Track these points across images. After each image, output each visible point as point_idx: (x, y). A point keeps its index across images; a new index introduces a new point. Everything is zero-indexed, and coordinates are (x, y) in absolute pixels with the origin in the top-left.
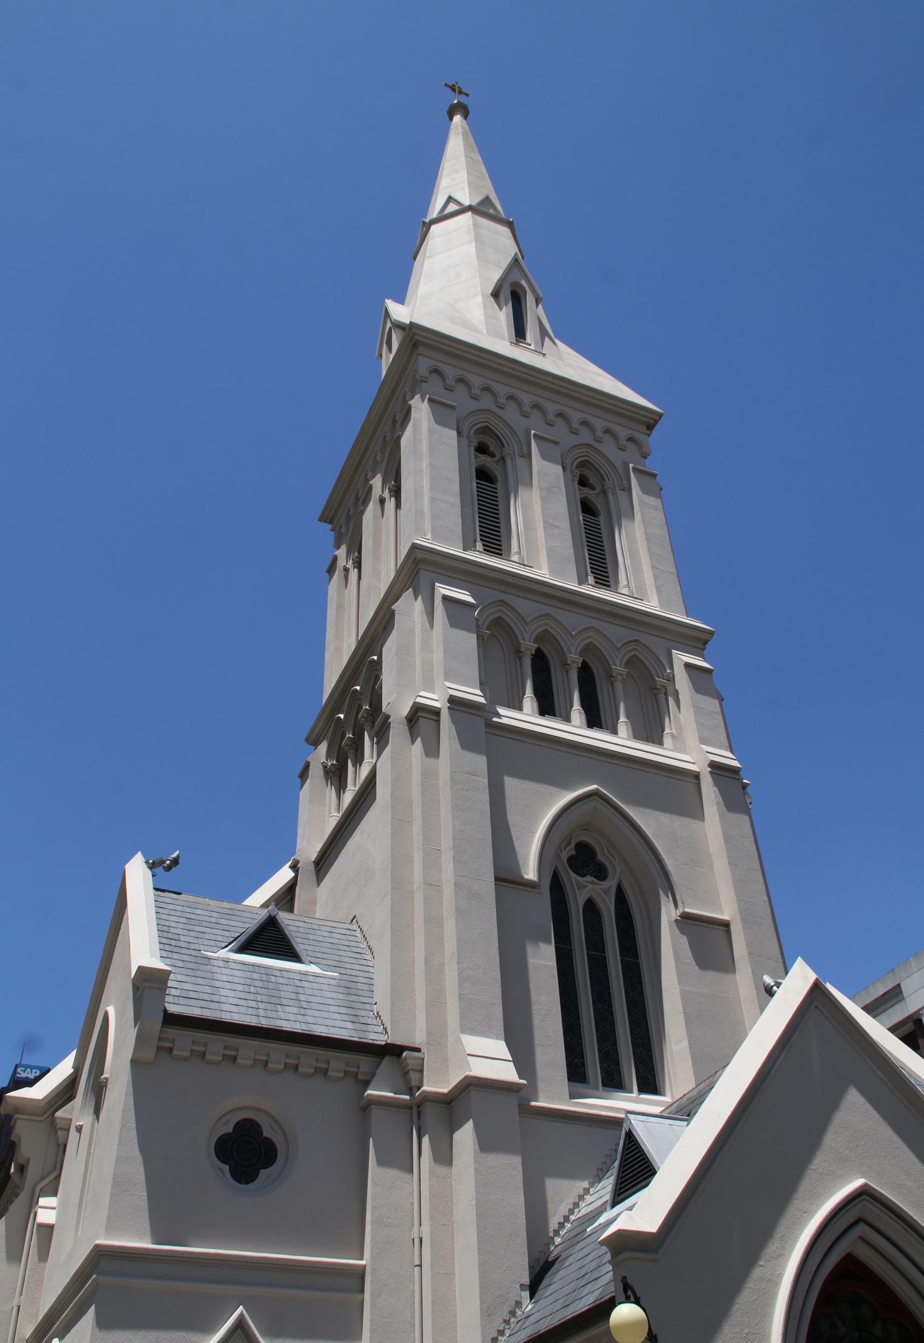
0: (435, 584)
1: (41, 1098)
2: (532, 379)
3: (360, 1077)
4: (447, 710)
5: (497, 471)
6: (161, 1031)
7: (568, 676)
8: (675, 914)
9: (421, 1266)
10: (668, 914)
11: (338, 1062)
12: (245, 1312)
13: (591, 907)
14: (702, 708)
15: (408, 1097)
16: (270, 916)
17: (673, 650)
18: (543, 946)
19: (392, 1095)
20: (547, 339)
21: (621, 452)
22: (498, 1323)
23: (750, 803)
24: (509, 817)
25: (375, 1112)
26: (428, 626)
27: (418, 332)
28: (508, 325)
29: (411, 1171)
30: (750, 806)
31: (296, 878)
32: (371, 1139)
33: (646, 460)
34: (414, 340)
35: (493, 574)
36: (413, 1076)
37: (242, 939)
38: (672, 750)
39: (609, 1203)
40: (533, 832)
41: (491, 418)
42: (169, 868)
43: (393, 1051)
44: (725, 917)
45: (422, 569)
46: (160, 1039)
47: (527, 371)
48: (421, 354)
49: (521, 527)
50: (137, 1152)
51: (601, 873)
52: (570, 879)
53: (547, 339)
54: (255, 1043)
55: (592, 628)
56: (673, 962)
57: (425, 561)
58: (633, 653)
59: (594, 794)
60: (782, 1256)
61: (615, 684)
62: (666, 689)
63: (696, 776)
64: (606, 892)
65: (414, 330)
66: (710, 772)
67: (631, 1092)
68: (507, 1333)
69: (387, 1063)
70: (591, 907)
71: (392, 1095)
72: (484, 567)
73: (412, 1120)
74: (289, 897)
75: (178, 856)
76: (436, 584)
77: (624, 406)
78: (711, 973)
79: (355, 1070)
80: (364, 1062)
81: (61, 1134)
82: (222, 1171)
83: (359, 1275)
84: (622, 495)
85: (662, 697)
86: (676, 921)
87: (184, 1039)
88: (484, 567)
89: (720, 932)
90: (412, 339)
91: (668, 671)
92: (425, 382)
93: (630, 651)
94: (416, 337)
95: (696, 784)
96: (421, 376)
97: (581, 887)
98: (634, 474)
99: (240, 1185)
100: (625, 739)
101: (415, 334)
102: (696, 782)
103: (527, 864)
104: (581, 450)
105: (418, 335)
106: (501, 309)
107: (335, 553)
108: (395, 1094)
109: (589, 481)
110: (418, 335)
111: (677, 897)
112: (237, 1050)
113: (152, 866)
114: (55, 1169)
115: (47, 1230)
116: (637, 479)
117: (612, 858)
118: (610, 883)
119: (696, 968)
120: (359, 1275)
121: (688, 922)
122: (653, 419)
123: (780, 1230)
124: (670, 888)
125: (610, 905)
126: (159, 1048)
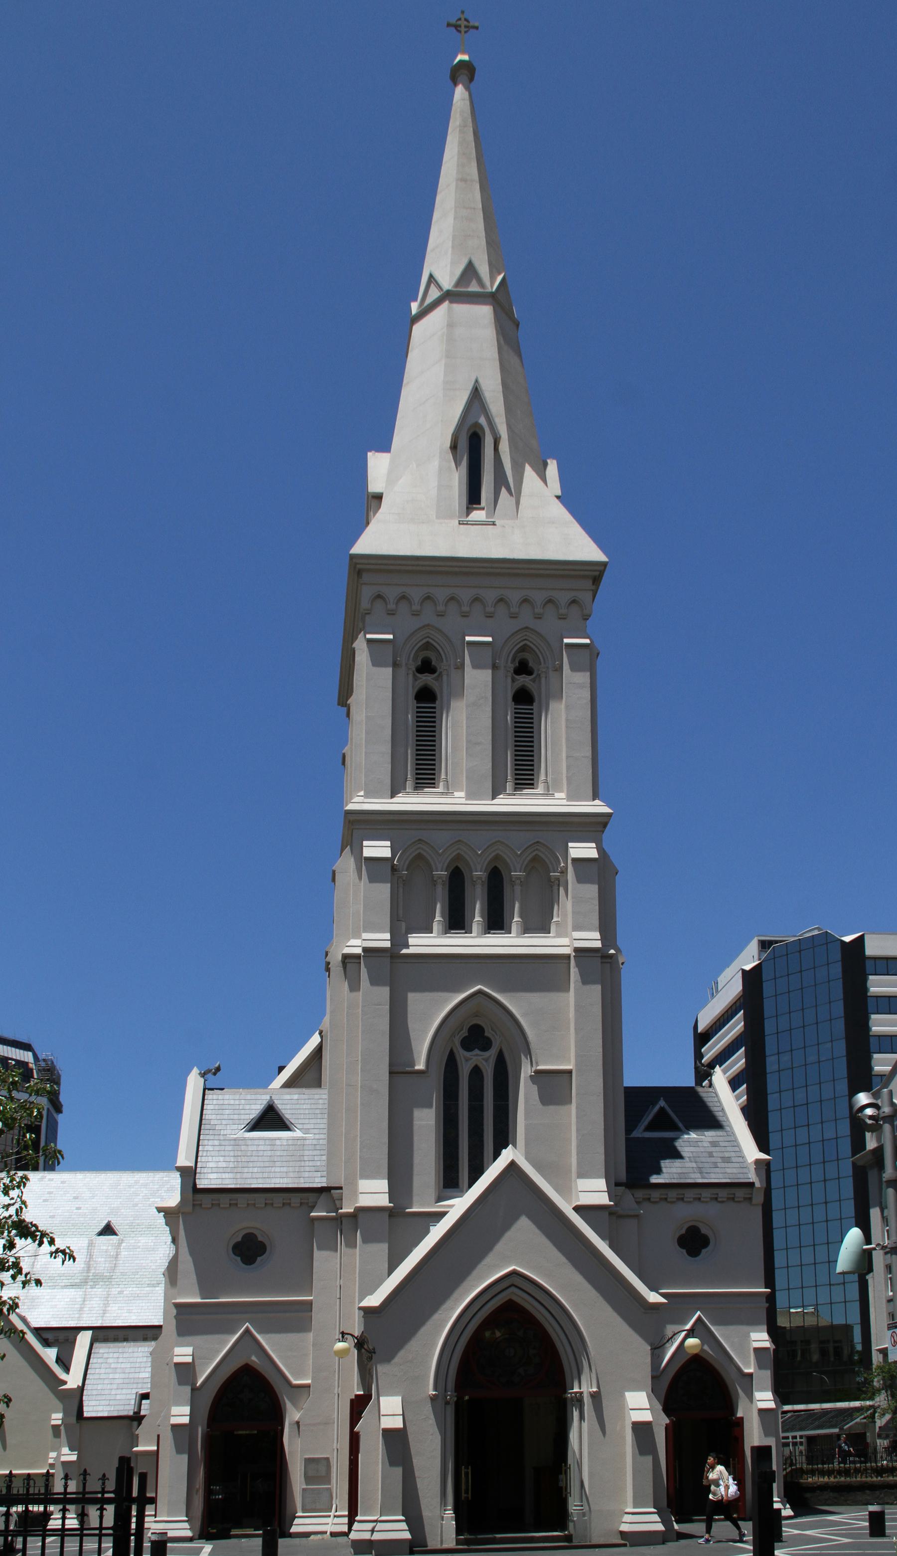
1: (174, 1206)
3: (310, 1205)
5: (435, 686)
6: (193, 1197)
9: (340, 1298)
10: (526, 1071)
11: (295, 1199)
12: (249, 1326)
13: (476, 1072)
14: (581, 897)
15: (335, 1214)
16: (269, 1105)
19: (325, 1214)
20: (504, 490)
23: (623, 964)
24: (410, 1025)
25: (316, 1223)
27: (358, 561)
28: (459, 496)
29: (337, 1251)
30: (621, 966)
31: (321, 1043)
34: (357, 570)
36: (337, 1202)
37: (253, 1123)
40: (427, 1033)
41: (433, 632)
42: (215, 1074)
45: (355, 829)
46: (193, 1200)
48: (365, 584)
49: (449, 750)
51: (486, 1045)
52: (461, 1054)
53: (504, 490)
54: (246, 1195)
55: (499, 841)
57: (359, 821)
58: (534, 853)
59: (480, 992)
60: (453, 1309)
61: (515, 887)
62: (559, 881)
64: (486, 1060)
69: (324, 1196)
70: (476, 1072)
71: (325, 1214)
74: (320, 1055)
75: (219, 1066)
78: (552, 1108)
79: (307, 1201)
80: (312, 1197)
82: (236, 1260)
86: (531, 1076)
87: (206, 1199)
89: (566, 1076)
90: (355, 567)
91: (562, 865)
92: (369, 614)
93: (532, 852)
94: (358, 566)
96: (365, 610)
97: (467, 1060)
99: (249, 1266)
101: (356, 564)
103: (420, 1057)
104: (519, 637)
105: (359, 564)
107: (343, 752)
108: (327, 1213)
109: (529, 664)
110: (359, 564)
111: (533, 1059)
112: (237, 1200)
113: (203, 1075)
117: (494, 1033)
118: (492, 1053)
122: (598, 571)
124: (528, 1052)
125: (487, 1068)
126: (194, 1205)
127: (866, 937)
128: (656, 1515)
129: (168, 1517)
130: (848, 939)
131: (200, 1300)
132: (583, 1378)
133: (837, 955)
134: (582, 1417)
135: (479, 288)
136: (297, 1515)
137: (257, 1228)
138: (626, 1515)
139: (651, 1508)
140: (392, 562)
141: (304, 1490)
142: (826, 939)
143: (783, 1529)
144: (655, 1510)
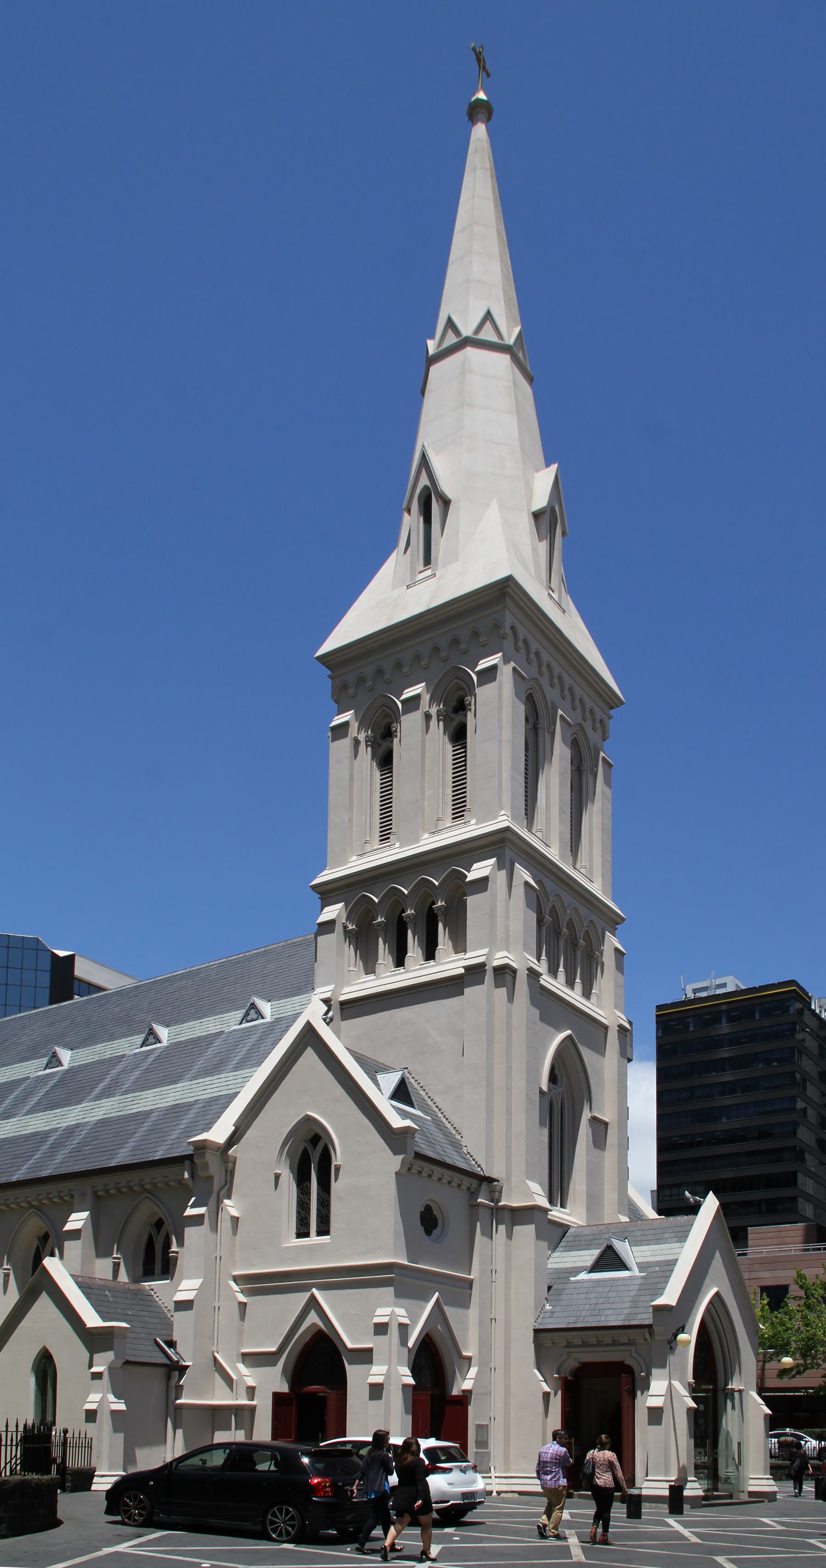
0: (514, 864)
2: (550, 635)
4: (526, 975)
7: (558, 943)
8: (589, 1115)
10: (586, 1115)
11: (467, 1182)
17: (607, 932)
18: (544, 1129)
19: (487, 1202)
21: (562, 699)
22: (538, 1313)
26: (508, 898)
27: (513, 586)
32: (478, 1224)
33: (605, 742)
34: (505, 590)
35: (540, 858)
38: (597, 1007)
39: (589, 1269)
43: (490, 1180)
44: (607, 1120)
47: (571, 651)
50: (400, 1220)
56: (585, 1143)
63: (606, 1028)
65: (510, 583)
66: (527, 974)
67: (556, 1206)
68: (541, 1316)
72: (535, 851)
73: (492, 1214)
76: (607, 932)
77: (606, 690)
78: (597, 1150)
81: (230, 1165)
83: (471, 1282)
84: (590, 777)
85: (595, 965)
86: (589, 1119)
88: (535, 851)
94: (509, 590)
95: (513, 976)
98: (603, 764)
100: (579, 995)
101: (508, 586)
102: (605, 1031)
105: (511, 588)
106: (540, 540)
114: (226, 1184)
115: (235, 1220)
116: (561, 727)
119: (593, 1147)
120: (471, 1282)
121: (594, 1120)
123: (696, 1305)
124: (590, 1100)
127: (77, 958)
128: (772, 1481)
129: (109, 1471)
130: (62, 953)
131: (406, 1263)
132: (734, 1379)
133: (47, 965)
134: (733, 1407)
135: (497, 338)
136: (96, 1473)
137: (435, 1202)
138: (750, 1480)
139: (120, 1471)
140: (525, 600)
141: (476, 1453)
142: (36, 946)
143: (814, 1490)
144: (772, 1477)
